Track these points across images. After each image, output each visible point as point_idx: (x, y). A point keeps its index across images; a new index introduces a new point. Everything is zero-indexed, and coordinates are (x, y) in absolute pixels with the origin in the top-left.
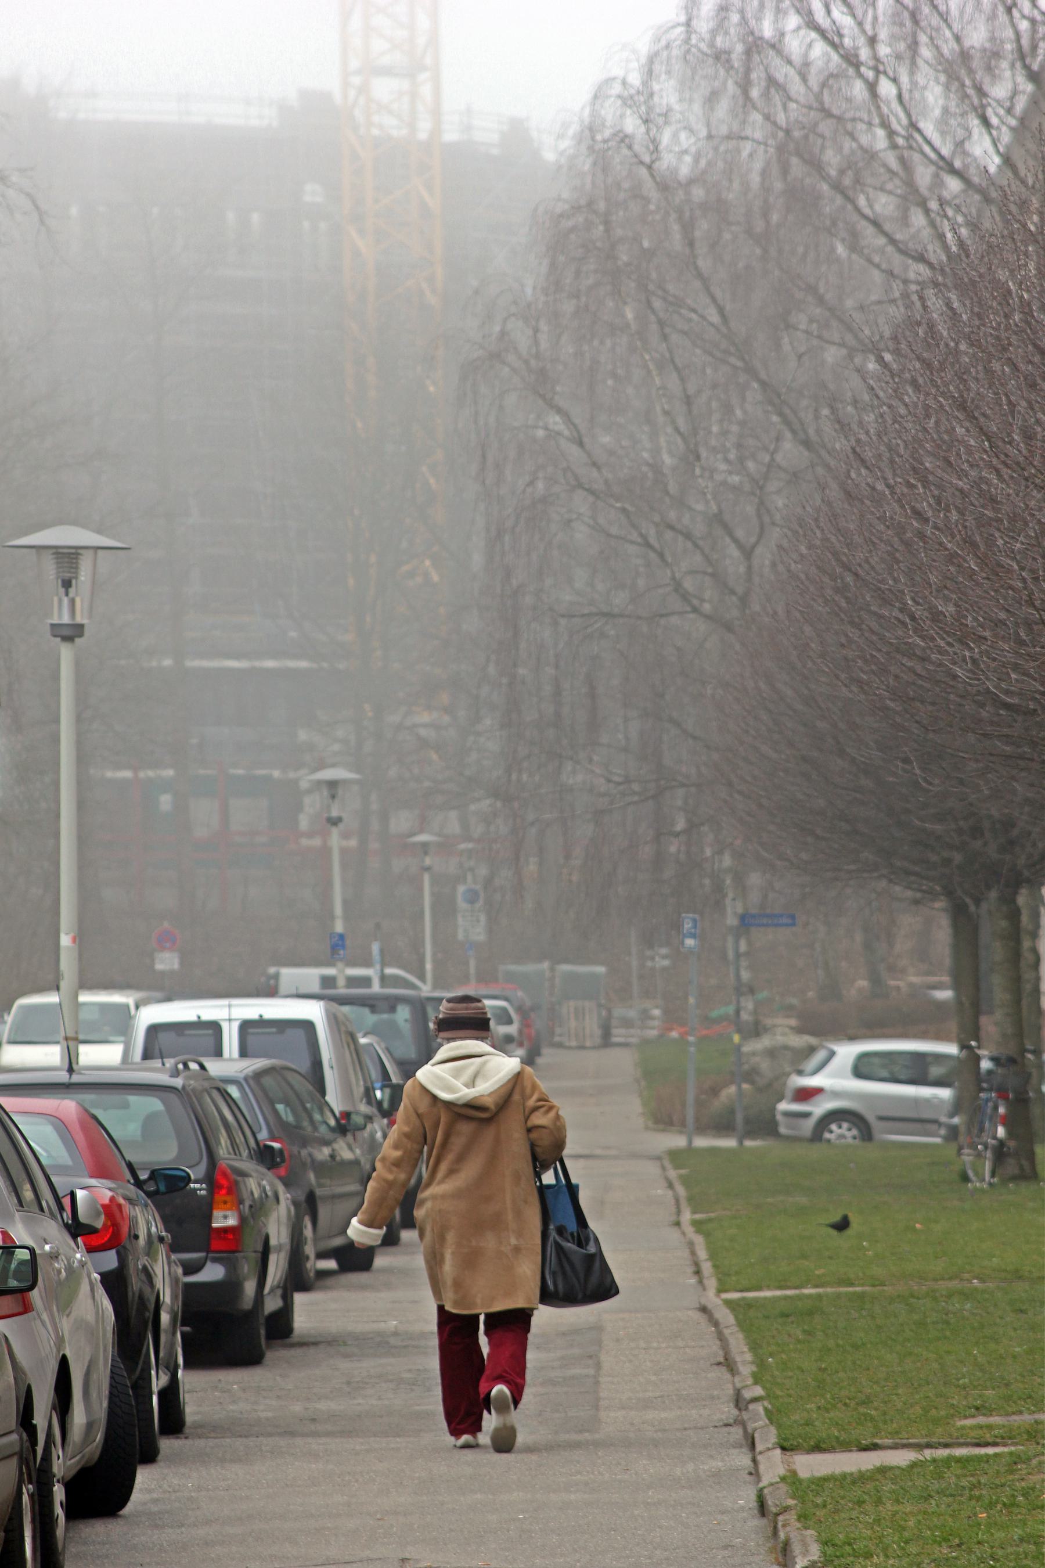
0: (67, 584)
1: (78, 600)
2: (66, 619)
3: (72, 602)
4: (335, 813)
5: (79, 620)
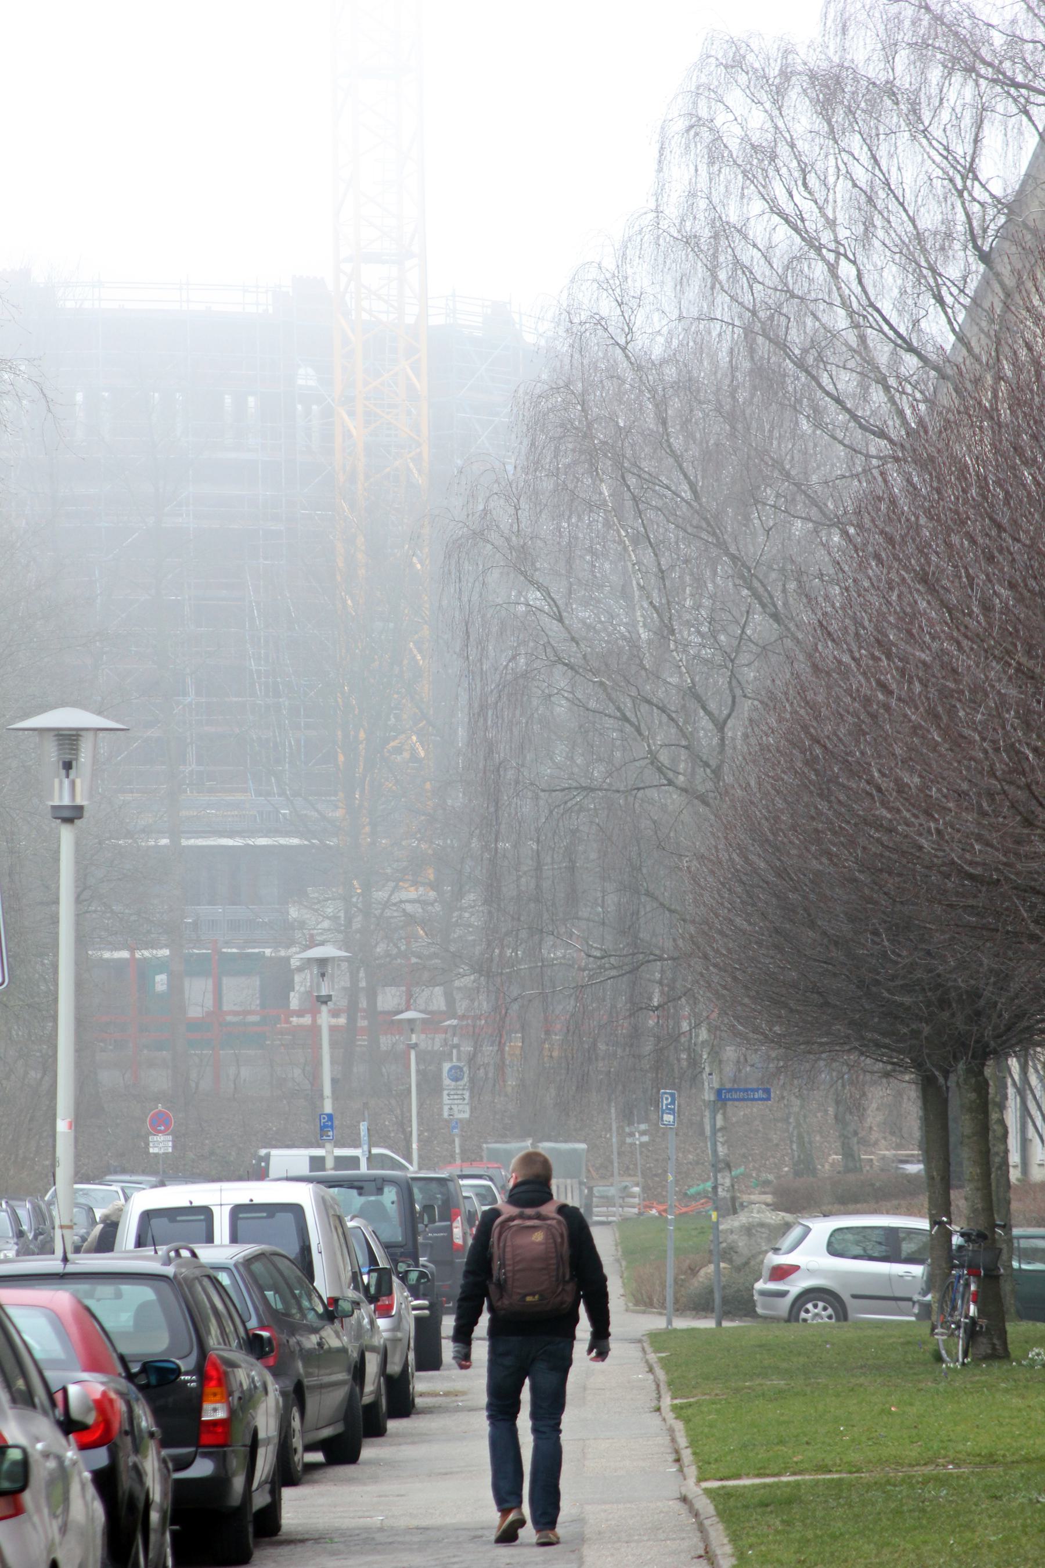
0: (68, 766)
1: (78, 782)
2: (66, 801)
3: (73, 784)
4: (324, 992)
5: (79, 801)
